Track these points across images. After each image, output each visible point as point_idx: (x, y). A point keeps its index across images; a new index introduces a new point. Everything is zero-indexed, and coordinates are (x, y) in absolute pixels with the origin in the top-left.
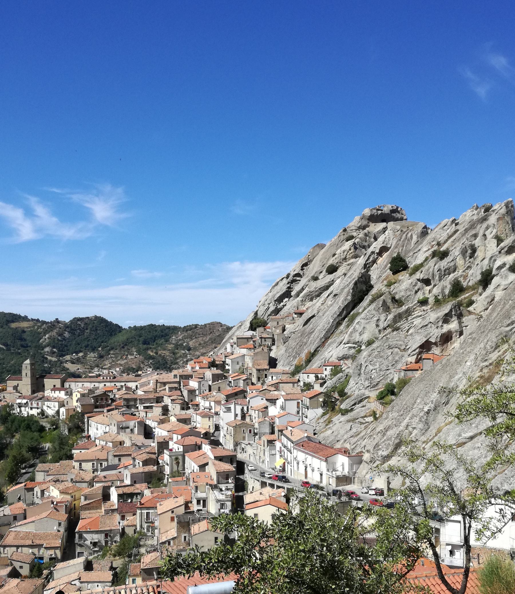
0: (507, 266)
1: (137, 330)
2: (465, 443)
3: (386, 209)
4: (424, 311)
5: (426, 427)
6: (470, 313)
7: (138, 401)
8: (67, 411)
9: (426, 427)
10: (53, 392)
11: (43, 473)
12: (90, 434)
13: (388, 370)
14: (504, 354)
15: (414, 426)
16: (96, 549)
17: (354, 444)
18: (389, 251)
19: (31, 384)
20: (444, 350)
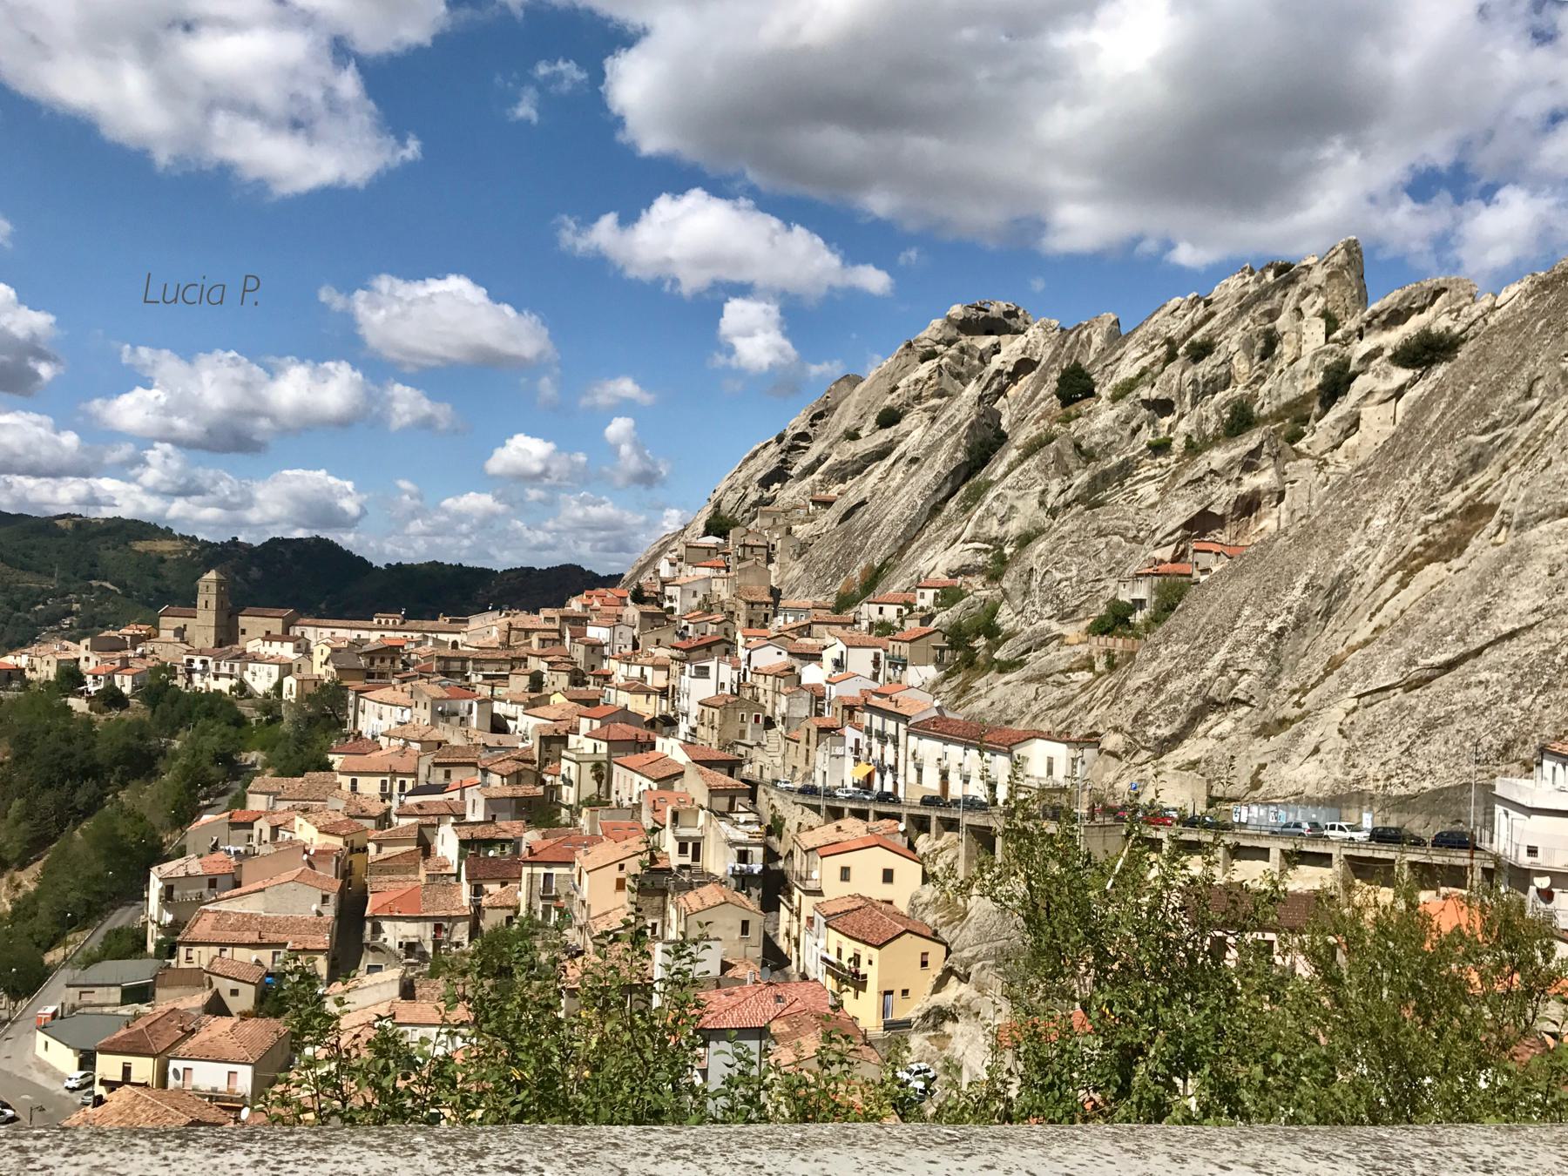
0: (1388, 352)
1: (399, 572)
2: (1429, 680)
3: (997, 309)
4: (1161, 466)
5: (1274, 667)
6: (1300, 455)
7: (470, 664)
8: (301, 682)
9: (1274, 667)
10: (267, 643)
11: (265, 797)
12: (359, 728)
13: (1098, 580)
14: (1479, 494)
15: (1242, 666)
16: (412, 960)
17: (1062, 722)
18: (1038, 369)
19: (217, 626)
20: (1242, 534)
